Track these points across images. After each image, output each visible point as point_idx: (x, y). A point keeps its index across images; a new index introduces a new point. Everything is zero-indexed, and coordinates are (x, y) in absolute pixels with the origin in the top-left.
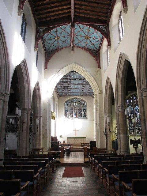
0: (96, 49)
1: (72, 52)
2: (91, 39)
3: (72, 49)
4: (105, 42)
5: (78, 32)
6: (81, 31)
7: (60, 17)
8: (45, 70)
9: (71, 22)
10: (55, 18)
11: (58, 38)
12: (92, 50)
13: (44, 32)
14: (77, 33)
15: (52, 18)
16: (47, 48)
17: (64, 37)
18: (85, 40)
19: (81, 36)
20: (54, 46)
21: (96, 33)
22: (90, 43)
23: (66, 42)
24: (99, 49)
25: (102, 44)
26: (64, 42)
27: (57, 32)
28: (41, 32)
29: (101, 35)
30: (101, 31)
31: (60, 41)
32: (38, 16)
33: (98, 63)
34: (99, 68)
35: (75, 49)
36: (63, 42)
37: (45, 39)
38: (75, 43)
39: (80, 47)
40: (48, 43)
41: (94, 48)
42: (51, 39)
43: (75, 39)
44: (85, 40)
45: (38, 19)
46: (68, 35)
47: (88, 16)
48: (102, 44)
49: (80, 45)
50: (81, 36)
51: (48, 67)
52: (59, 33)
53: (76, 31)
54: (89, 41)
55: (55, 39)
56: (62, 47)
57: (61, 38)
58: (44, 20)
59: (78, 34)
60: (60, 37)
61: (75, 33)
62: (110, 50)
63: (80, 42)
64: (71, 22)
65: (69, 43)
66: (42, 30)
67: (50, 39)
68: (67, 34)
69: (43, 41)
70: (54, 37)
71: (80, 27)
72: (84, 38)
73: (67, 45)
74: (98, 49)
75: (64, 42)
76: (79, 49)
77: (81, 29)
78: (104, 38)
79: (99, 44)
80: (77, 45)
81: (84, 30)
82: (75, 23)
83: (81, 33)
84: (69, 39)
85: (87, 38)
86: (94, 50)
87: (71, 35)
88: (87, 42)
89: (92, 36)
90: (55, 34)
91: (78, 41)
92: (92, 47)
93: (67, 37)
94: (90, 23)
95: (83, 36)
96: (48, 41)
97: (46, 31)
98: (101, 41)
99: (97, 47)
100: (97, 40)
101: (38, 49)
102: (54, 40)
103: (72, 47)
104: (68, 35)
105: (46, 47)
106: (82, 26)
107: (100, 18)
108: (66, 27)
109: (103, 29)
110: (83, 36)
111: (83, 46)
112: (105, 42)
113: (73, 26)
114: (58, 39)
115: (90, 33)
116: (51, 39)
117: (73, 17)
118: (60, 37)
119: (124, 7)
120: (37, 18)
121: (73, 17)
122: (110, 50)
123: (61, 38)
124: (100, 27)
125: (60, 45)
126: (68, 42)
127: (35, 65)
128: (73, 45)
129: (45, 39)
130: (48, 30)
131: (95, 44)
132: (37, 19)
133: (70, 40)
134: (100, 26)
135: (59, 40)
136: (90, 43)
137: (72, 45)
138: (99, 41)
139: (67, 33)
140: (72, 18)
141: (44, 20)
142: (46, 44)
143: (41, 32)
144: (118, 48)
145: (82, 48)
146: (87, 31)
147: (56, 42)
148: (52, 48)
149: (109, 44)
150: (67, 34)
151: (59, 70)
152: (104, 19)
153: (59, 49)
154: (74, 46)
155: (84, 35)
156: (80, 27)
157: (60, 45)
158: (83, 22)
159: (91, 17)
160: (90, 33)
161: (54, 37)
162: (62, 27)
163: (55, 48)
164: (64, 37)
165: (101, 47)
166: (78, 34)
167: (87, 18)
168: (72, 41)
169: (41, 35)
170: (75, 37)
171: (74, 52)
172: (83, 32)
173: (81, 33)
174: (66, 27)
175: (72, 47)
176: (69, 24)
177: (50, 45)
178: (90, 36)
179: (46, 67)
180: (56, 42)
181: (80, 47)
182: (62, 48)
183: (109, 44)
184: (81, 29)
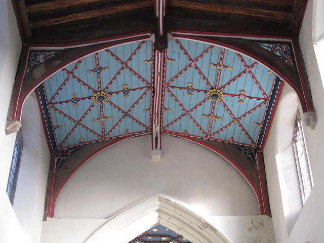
0: (249, 142)
1: (156, 157)
2: (229, 101)
3: (156, 144)
4: (290, 102)
5: (181, 73)
6: (191, 70)
7: (114, 11)
8: (45, 219)
9: (156, 32)
10: (96, 18)
11: (101, 95)
12: (233, 145)
13: (51, 65)
14: (176, 77)
15: (82, 16)
16: (60, 135)
17: (126, 92)
18: (208, 103)
19: (190, 89)
20: (84, 130)
21: (249, 76)
22: (227, 119)
23: (135, 113)
24: (259, 141)
25: (266, 135)
26: (126, 114)
27: (98, 70)
28: (38, 64)
29: (265, 75)
30: (268, 60)
31: (108, 109)
32: (33, 7)
33: (259, 195)
34: (262, 213)
35: (167, 140)
36: (121, 115)
37: (53, 98)
38: (168, 117)
39: (185, 136)
40: (65, 115)
41: (241, 138)
42: (77, 99)
43: (169, 102)
44: (208, 103)
45: (32, 17)
46: (143, 84)
47: (219, 10)
48: (273, 116)
49: (184, 125)
50: (190, 89)
51: (59, 208)
52: (106, 76)
53: (172, 68)
54: (220, 110)
55: (89, 98)
56: (116, 132)
57: (114, 98)
58: (53, 22)
59: (181, 81)
60: (110, 94)
61: (167, 79)
62: (313, 128)
63: (186, 113)
64: (156, 32)
65: (144, 117)
66: (41, 58)
67: (72, 101)
68: (136, 82)
69: (41, 94)
70: (86, 92)
71: (186, 53)
72: (202, 96)
73: (136, 128)
74: (255, 140)
75: (126, 114)
76: (182, 143)
77: (190, 59)
78: (282, 86)
79: (261, 119)
80: (176, 127)
81: (203, 64)
82: (169, 35)
83: (191, 77)
84: (145, 103)
85: (215, 96)
86: (243, 146)
87: (151, 87)
88: (212, 115)
89: (232, 88)
90: (91, 79)
91: (179, 112)
92: (234, 134)
93: (134, 95)
94: (224, 33)
95: (199, 91)
96: (64, 108)
97: (58, 62)
98: (269, 107)
99: (255, 133)
100: (253, 103)
101: (19, 124)
102: (87, 103)
103: (154, 136)
104: (143, 84)
105: (56, 132)
106: (195, 45)
107: (266, 14)
108: (141, 98)
109: (278, 53)
110: (199, 91)
111: (197, 132)
112: (290, 102)
113: (161, 45)
114: (101, 98)
115: (226, 76)
116: (75, 100)
117: (160, 13)
118: (110, 94)
119: (305, 110)
120: (29, 14)
121: (160, 13)
122: (313, 128)
123: (114, 98)
124: (265, 46)
125: (109, 125)
126: (141, 113)
127: (6, 197)
128: (158, 129)
129: (53, 98)
130: (64, 58)
131: (245, 121)
132: (26, 18)
133: (148, 106)
134: (267, 43)
135: (106, 105)
136: (227, 114)
137: (156, 129)
138: (260, 106)
139: (139, 77)
140: (158, 18)
141: (53, 22)
142: (54, 115)
143: (38, 64)
144: (296, 225)
145: (195, 139)
146: (206, 119)
147: (95, 112)
148: (80, 136)
149: (307, 104)
150: (136, 82)
151: (105, 221)
152: (279, 15)
153: (105, 142)
154: (163, 131)
155: (203, 85)
156: (186, 53)
157: (109, 125)
158: (201, 31)
159: (231, 11)
160: (226, 76)
161: (86, 92)
162: (117, 49)
163: (91, 137)
164: (126, 92)
165: (268, 132)
166: (181, 81)
167: (214, 17)
168: (156, 112)
169: (37, 73)
170: (167, 94)
171: (162, 157)
172: (200, 73)
173: (191, 77)
174: (141, 98)
175: (154, 136)
176: (148, 37)
177: (70, 125)
178: (226, 90)
179: (49, 210)
180: (95, 112)
181: (185, 136)
182: (119, 139)
183: (307, 104)
184: (190, 59)
